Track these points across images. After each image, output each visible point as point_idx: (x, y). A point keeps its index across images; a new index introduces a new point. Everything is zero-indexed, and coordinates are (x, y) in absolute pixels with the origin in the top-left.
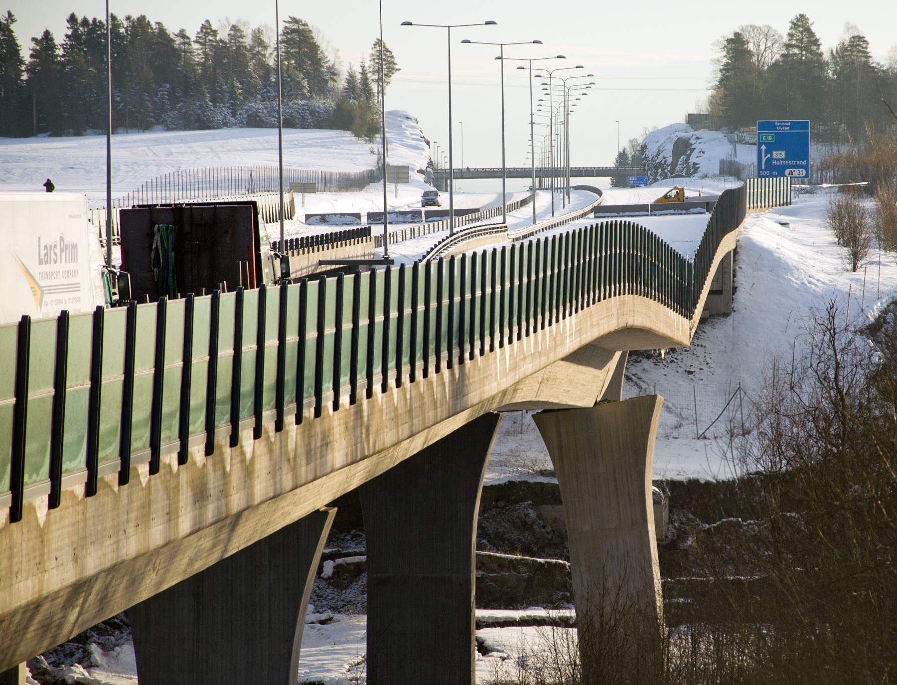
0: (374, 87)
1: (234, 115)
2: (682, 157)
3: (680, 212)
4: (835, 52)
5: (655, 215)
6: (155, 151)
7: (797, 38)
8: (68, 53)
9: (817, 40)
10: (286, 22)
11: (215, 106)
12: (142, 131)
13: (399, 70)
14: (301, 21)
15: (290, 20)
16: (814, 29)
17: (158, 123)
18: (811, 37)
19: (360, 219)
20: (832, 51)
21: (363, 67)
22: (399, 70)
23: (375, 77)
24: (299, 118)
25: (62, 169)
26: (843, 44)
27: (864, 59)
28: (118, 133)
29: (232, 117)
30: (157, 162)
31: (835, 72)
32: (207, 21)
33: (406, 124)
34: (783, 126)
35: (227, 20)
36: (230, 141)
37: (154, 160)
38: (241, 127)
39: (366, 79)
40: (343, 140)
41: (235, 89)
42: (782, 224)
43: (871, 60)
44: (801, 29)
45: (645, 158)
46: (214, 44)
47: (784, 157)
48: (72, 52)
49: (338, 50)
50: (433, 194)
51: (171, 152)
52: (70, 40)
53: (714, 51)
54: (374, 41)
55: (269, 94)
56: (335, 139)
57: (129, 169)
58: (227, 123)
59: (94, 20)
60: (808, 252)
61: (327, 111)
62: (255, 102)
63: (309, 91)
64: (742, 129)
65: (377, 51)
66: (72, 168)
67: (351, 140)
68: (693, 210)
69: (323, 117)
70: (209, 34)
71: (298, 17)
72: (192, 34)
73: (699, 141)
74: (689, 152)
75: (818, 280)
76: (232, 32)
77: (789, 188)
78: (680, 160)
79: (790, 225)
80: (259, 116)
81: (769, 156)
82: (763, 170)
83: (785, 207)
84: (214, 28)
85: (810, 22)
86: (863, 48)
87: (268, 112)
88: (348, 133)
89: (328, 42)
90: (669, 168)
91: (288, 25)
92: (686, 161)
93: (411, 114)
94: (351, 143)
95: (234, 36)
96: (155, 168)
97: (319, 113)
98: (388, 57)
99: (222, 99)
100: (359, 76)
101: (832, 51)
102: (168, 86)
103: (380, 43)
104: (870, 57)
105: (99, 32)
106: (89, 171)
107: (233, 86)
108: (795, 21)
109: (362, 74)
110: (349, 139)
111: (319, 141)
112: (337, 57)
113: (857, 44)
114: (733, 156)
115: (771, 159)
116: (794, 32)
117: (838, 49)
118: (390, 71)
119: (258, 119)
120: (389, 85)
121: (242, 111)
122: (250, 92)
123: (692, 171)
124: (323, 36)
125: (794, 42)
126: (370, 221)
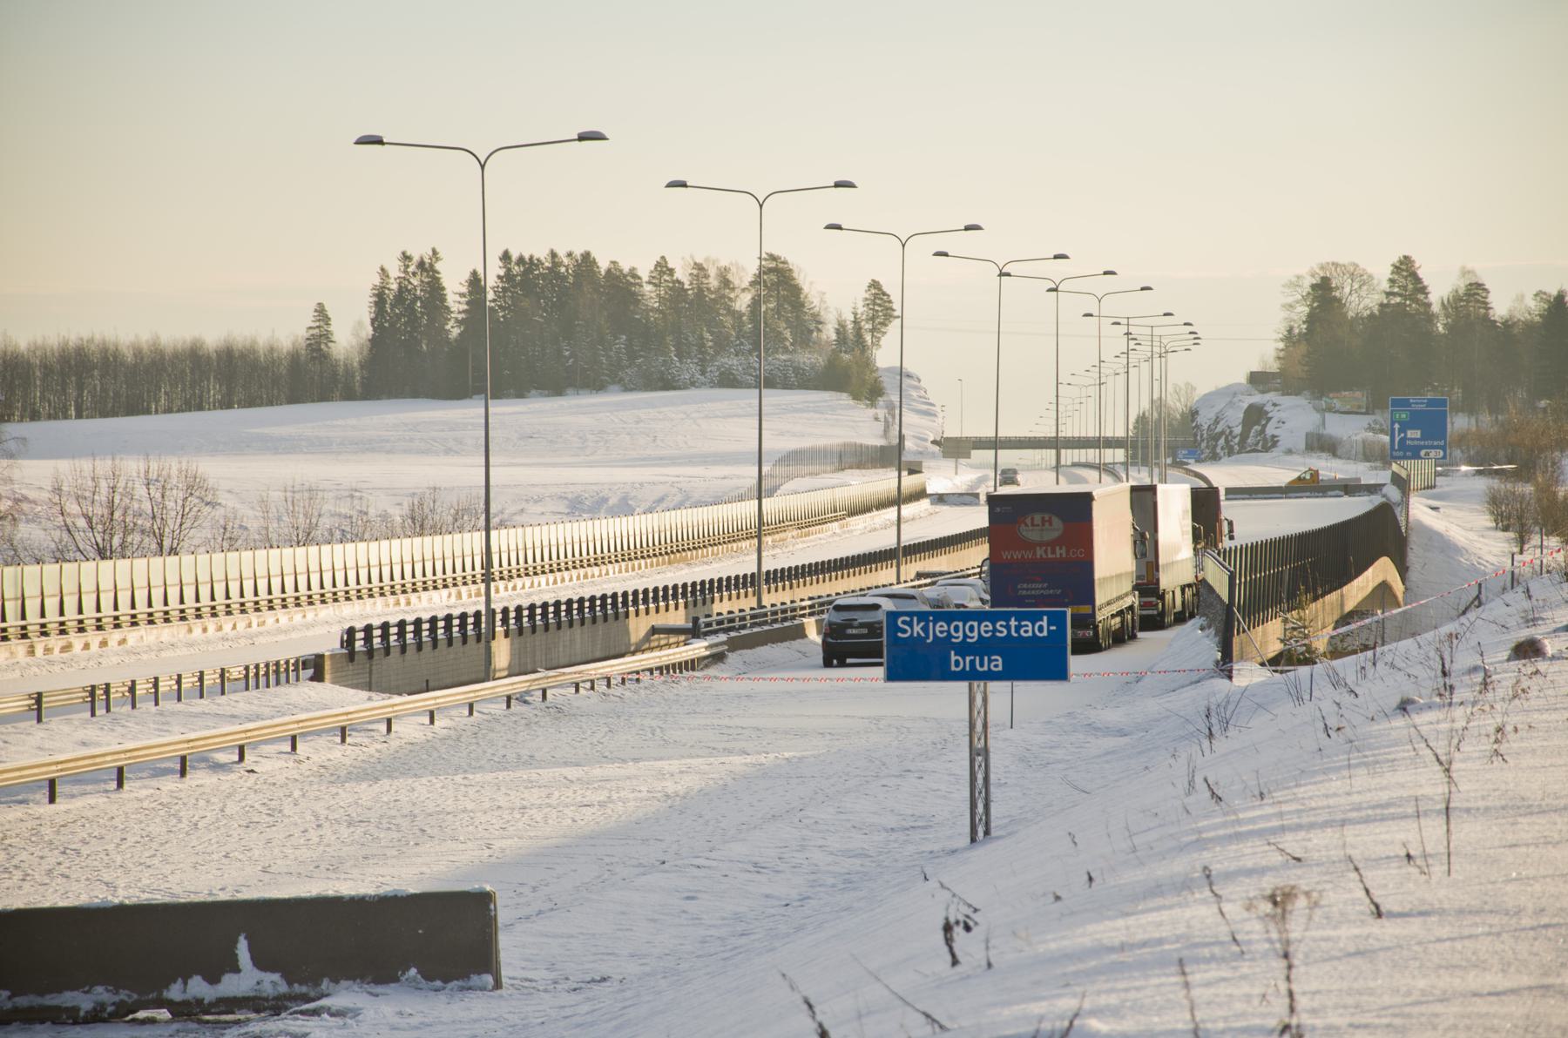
0: (868, 338)
1: (703, 373)
2: (1256, 427)
4: (1446, 302)
5: (1290, 498)
8: (499, 297)
9: (1425, 288)
11: (681, 361)
16: (1421, 273)
17: (614, 383)
21: (855, 314)
23: (869, 326)
25: (520, 439)
26: (1457, 291)
27: (1482, 311)
28: (567, 395)
31: (1445, 325)
32: (663, 258)
34: (1419, 402)
35: (692, 257)
38: (712, 387)
39: (860, 328)
42: (1433, 508)
43: (1491, 312)
44: (1405, 274)
45: (1197, 426)
46: (671, 285)
47: (1419, 436)
48: (504, 297)
49: (824, 293)
52: (502, 282)
59: (531, 258)
60: (1472, 535)
61: (813, 367)
64: (1331, 395)
70: (664, 273)
71: (776, 253)
72: (644, 274)
73: (1277, 408)
74: (1264, 422)
76: (695, 272)
81: (1402, 435)
84: (670, 265)
85: (1417, 265)
88: (845, 395)
89: (811, 283)
90: (1237, 440)
92: (1263, 431)
94: (854, 408)
95: (697, 276)
96: (628, 437)
97: (804, 370)
99: (689, 353)
100: (850, 326)
102: (624, 337)
105: (537, 272)
107: (702, 338)
108: (1398, 265)
109: (854, 322)
112: (822, 301)
113: (1475, 292)
116: (1396, 277)
121: (712, 368)
122: (722, 344)
123: (1269, 444)
125: (1396, 290)
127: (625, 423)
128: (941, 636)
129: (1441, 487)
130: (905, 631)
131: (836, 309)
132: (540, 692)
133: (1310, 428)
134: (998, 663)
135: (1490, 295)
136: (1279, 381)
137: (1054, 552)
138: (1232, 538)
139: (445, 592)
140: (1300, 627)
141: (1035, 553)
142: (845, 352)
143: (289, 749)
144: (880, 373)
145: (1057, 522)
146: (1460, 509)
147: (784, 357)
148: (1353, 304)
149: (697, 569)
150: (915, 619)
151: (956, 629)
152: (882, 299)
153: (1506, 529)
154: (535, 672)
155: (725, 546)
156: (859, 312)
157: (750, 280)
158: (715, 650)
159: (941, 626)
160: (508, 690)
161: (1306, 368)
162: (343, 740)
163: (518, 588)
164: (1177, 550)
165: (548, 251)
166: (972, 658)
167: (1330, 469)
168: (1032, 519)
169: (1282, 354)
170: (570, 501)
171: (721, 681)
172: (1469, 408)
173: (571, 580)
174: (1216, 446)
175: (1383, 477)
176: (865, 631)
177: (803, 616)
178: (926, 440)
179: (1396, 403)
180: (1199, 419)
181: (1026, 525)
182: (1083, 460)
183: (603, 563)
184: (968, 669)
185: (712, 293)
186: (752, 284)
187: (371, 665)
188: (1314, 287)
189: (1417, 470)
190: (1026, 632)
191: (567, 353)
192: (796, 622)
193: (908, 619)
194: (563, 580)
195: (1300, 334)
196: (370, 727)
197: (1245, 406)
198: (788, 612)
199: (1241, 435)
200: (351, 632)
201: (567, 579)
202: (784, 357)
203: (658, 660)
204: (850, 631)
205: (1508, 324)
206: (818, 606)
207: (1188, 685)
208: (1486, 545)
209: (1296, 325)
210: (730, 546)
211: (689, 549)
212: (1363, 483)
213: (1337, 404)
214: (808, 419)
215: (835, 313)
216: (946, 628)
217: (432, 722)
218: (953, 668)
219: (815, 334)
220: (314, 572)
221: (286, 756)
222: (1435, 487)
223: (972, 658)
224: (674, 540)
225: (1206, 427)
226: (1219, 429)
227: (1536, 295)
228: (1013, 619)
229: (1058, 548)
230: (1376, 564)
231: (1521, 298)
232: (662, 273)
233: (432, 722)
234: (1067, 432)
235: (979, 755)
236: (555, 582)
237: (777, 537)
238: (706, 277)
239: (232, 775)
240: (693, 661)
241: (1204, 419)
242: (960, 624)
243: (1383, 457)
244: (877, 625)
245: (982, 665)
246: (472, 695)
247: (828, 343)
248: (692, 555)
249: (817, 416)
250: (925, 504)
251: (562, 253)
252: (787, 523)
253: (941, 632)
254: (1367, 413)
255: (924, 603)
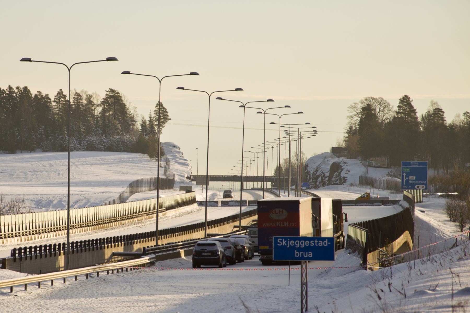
0: (156, 129)
1: (80, 144)
2: (336, 173)
3: (369, 204)
5: (358, 206)
6: (42, 164)
7: (403, 108)
9: (415, 110)
10: (107, 91)
12: (30, 152)
13: (170, 119)
14: (116, 91)
15: (109, 90)
16: (413, 104)
18: (411, 108)
19: (218, 204)
20: (423, 116)
21: (150, 117)
22: (170, 119)
23: (156, 123)
24: (115, 146)
26: (429, 112)
28: (17, 153)
29: (79, 145)
30: (47, 170)
31: (423, 128)
32: (61, 90)
33: (174, 150)
34: (415, 162)
35: (75, 90)
36: (81, 159)
37: (44, 169)
38: (84, 150)
39: (153, 124)
40: (144, 159)
41: (81, 129)
43: (445, 122)
46: (64, 103)
47: (415, 179)
49: (136, 108)
50: (229, 192)
51: (51, 164)
53: (349, 111)
54: (157, 102)
55: (98, 132)
56: (139, 159)
57: (33, 174)
58: (76, 148)
60: (441, 224)
61: (131, 142)
62: (92, 136)
63: (121, 131)
64: (371, 159)
65: (158, 108)
66: (2, 173)
67: (148, 159)
68: (375, 204)
69: (129, 145)
70: (62, 97)
71: (114, 89)
72: (52, 97)
74: (340, 171)
75: (447, 235)
76: (76, 97)
77: (422, 195)
78: (335, 175)
79: (425, 212)
80: (94, 145)
81: (407, 178)
82: (404, 185)
83: (420, 204)
84: (64, 94)
85: (411, 100)
86: (441, 115)
87: (99, 142)
88: (146, 155)
89: (130, 103)
90: (327, 179)
91: (108, 93)
93: (176, 144)
94: (149, 161)
95: (77, 99)
96: (46, 173)
98: (164, 112)
100: (148, 123)
101: (423, 116)
102: (43, 127)
103: (160, 104)
104: (445, 120)
106: (11, 174)
107: (79, 127)
108: (402, 99)
110: (147, 158)
111: (130, 159)
112: (135, 111)
114: (366, 174)
115: (408, 180)
116: (401, 105)
117: (426, 115)
118: (165, 120)
119: (93, 146)
120: (164, 128)
122: (89, 130)
124: (127, 99)
125: (401, 111)
126: (222, 205)
127: (45, 166)
128: (292, 245)
129: (425, 202)
130: (280, 244)
131: (142, 116)
132: (96, 274)
133: (361, 174)
134: (311, 255)
135: (444, 114)
136: (346, 152)
137: (283, 224)
138: (346, 221)
139: (16, 238)
140: (386, 254)
141: (276, 225)
142: (146, 135)
143: (24, 289)
144: (162, 145)
145: (285, 212)
146: (433, 212)
147: (117, 137)
148: (380, 117)
149: (110, 232)
150: (283, 240)
151: (297, 243)
152: (163, 111)
153: (454, 221)
154: (95, 265)
155: (119, 222)
156: (152, 116)
157: (101, 101)
158: (152, 260)
159: (292, 242)
160: (64, 276)
161: (359, 146)
162: (39, 287)
163: (43, 238)
164: (327, 225)
165: (7, 86)
166: (302, 253)
167: (375, 193)
168: (275, 211)
169: (346, 139)
170: (36, 202)
171: (156, 272)
172: (435, 167)
173: (62, 235)
174: (317, 181)
175: (399, 197)
176: (210, 254)
177: (180, 248)
178: (183, 177)
179: (404, 164)
180: (308, 169)
181: (273, 213)
182: (255, 187)
183: (74, 228)
184: (301, 256)
185: (84, 107)
186: (103, 103)
187: (21, 263)
188: (364, 109)
189: (416, 193)
190: (320, 244)
191: (17, 134)
192: (178, 251)
193: (281, 239)
194: (59, 235)
195: (356, 130)
196: (45, 283)
197: (331, 163)
198: (174, 247)
199: (329, 176)
200: (15, 250)
201: (60, 234)
202: (117, 137)
203: (133, 263)
204: (204, 254)
205: (453, 127)
206: (186, 245)
207: (350, 273)
208: (446, 227)
209: (354, 126)
210: (121, 222)
211: (99, 224)
212: (390, 199)
213: (374, 163)
214: (129, 166)
215: (141, 117)
216: (294, 243)
217: (65, 282)
218: (296, 256)
219: (131, 127)
220: (10, 225)
221: (23, 291)
222: (422, 202)
223: (302, 253)
224: (93, 220)
225: (312, 172)
226: (318, 173)
227: (465, 114)
228: (316, 240)
229: (285, 222)
230: (404, 233)
231: (458, 116)
232: (60, 97)
233: (65, 282)
234: (247, 173)
235: (304, 285)
236: (56, 236)
237: (139, 218)
238: (82, 99)
239: (11, 296)
240: (144, 264)
241: (311, 169)
242: (299, 241)
243: (397, 189)
244: (214, 252)
245: (305, 255)
246: (40, 279)
247: (137, 130)
248: (107, 225)
249: (133, 164)
250: (195, 205)
251: (14, 87)
252: (143, 213)
253: (292, 244)
254: (387, 168)
255: (230, 244)
